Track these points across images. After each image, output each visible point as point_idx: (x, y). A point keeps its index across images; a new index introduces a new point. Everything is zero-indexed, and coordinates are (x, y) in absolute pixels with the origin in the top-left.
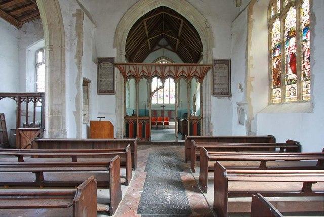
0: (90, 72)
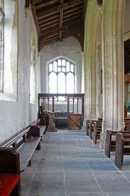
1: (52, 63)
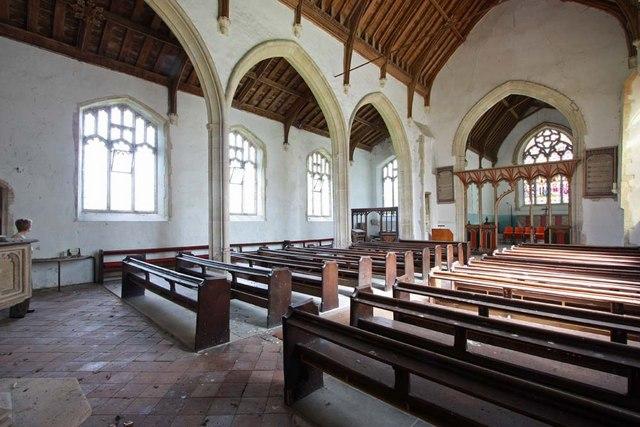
0: (430, 185)
1: (386, 165)
